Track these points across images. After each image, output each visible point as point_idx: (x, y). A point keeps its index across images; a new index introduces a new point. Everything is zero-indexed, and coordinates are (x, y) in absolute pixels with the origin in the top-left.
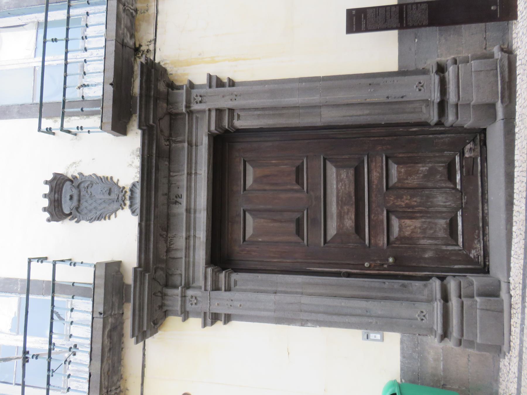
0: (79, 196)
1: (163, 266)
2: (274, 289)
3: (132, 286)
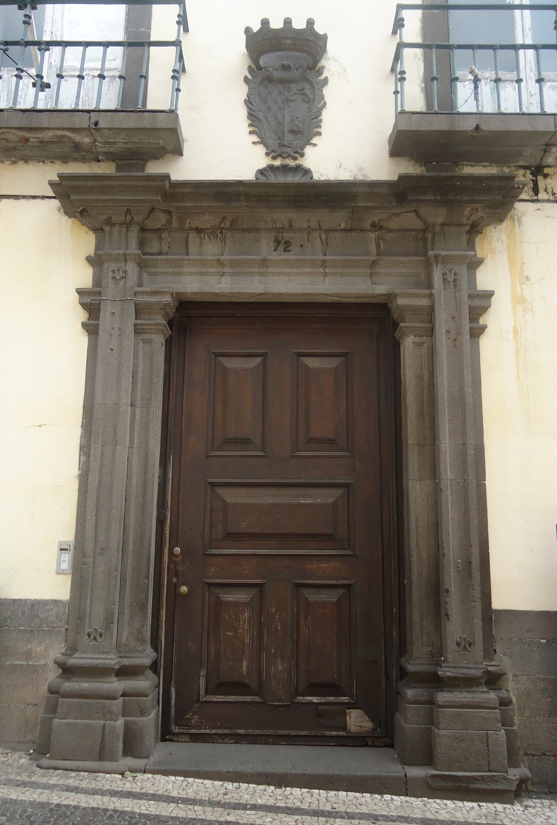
0: (290, 81)
1: (175, 224)
2: (138, 403)
3: (140, 174)
